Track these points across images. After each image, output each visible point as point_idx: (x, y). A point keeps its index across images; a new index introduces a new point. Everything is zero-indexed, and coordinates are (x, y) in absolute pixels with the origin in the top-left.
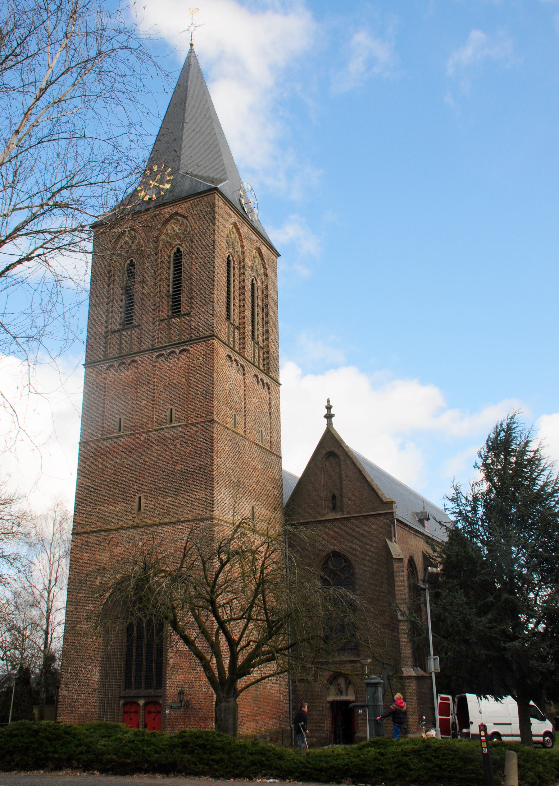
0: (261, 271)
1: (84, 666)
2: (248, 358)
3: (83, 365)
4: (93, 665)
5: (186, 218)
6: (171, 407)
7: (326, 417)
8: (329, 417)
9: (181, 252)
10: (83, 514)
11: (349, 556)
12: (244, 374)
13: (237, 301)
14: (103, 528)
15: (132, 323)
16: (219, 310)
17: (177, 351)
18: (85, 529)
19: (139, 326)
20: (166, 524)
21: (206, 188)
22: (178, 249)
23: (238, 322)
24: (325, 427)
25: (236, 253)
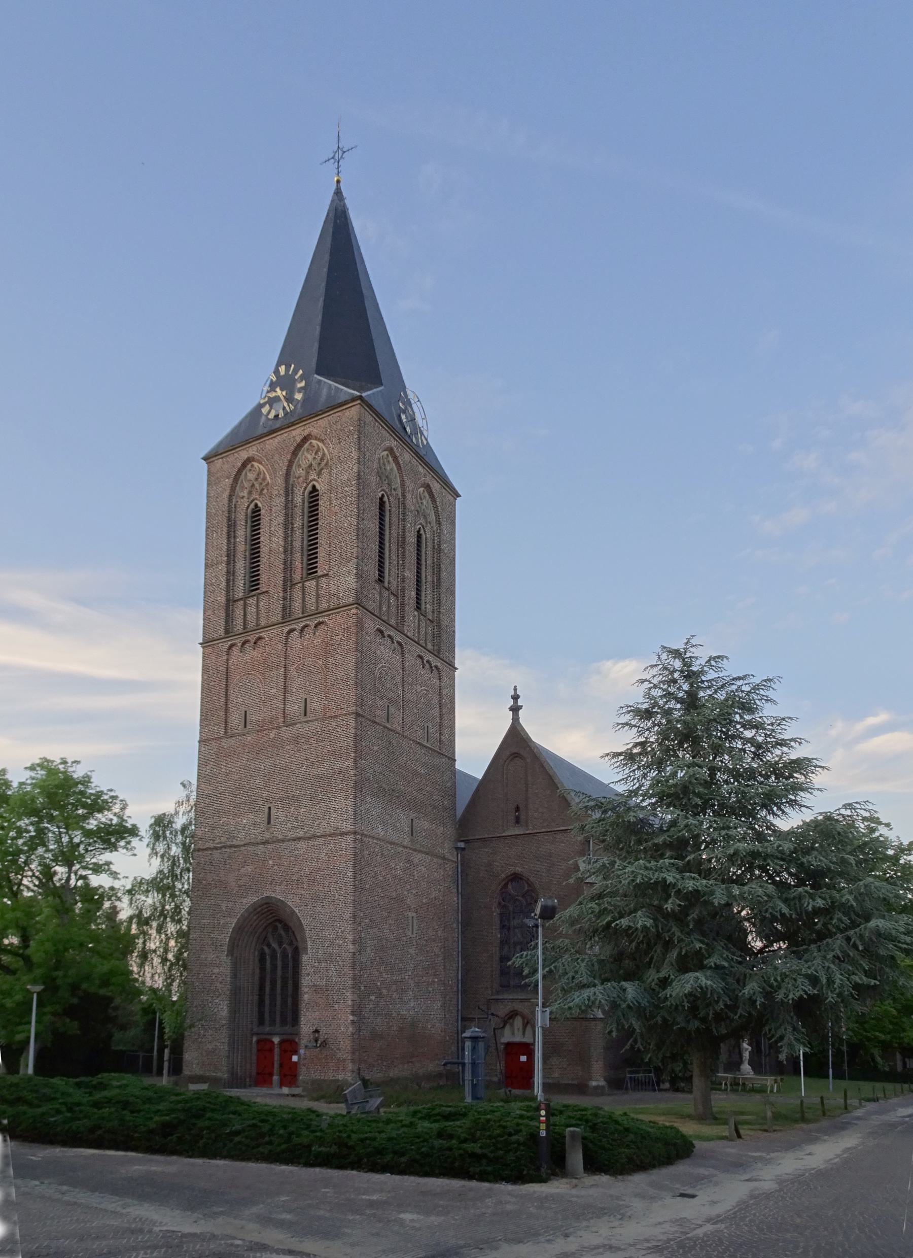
0: (432, 517)
1: (210, 999)
2: (409, 634)
3: (200, 644)
4: (220, 998)
5: (322, 441)
6: (305, 697)
7: (511, 709)
8: (515, 709)
9: (318, 490)
10: (206, 828)
11: (532, 879)
12: (403, 653)
13: (394, 557)
14: (228, 843)
15: (258, 589)
16: (365, 569)
17: (312, 625)
18: (207, 845)
19: (267, 592)
20: (299, 839)
21: (347, 398)
22: (314, 487)
23: (395, 585)
24: (509, 722)
25: (393, 492)
